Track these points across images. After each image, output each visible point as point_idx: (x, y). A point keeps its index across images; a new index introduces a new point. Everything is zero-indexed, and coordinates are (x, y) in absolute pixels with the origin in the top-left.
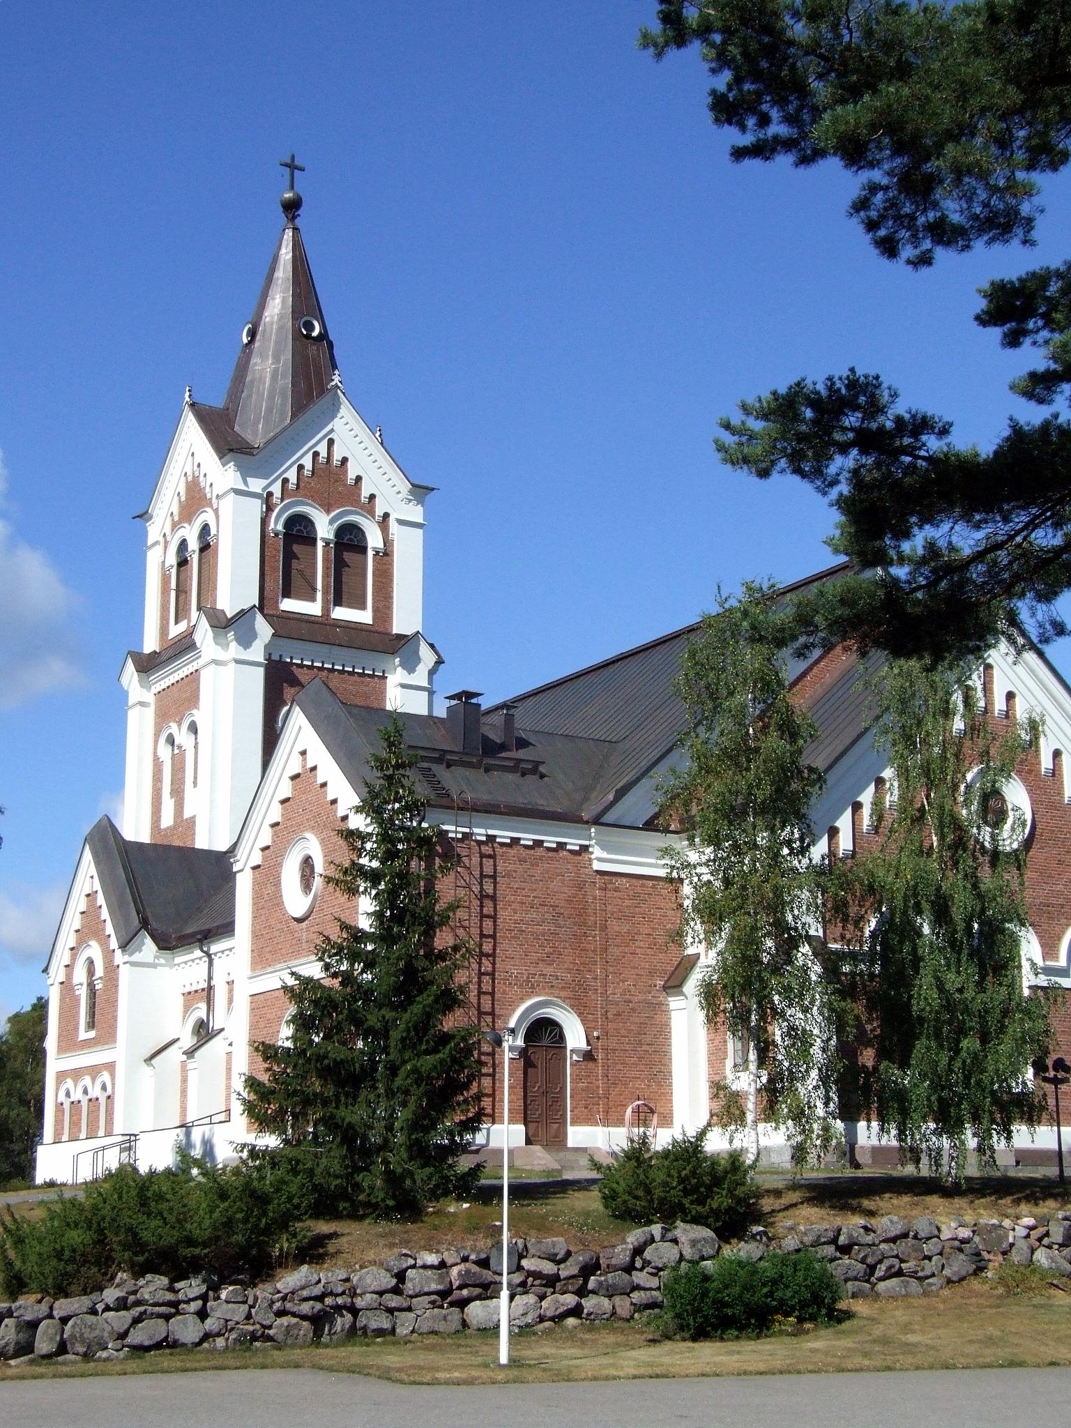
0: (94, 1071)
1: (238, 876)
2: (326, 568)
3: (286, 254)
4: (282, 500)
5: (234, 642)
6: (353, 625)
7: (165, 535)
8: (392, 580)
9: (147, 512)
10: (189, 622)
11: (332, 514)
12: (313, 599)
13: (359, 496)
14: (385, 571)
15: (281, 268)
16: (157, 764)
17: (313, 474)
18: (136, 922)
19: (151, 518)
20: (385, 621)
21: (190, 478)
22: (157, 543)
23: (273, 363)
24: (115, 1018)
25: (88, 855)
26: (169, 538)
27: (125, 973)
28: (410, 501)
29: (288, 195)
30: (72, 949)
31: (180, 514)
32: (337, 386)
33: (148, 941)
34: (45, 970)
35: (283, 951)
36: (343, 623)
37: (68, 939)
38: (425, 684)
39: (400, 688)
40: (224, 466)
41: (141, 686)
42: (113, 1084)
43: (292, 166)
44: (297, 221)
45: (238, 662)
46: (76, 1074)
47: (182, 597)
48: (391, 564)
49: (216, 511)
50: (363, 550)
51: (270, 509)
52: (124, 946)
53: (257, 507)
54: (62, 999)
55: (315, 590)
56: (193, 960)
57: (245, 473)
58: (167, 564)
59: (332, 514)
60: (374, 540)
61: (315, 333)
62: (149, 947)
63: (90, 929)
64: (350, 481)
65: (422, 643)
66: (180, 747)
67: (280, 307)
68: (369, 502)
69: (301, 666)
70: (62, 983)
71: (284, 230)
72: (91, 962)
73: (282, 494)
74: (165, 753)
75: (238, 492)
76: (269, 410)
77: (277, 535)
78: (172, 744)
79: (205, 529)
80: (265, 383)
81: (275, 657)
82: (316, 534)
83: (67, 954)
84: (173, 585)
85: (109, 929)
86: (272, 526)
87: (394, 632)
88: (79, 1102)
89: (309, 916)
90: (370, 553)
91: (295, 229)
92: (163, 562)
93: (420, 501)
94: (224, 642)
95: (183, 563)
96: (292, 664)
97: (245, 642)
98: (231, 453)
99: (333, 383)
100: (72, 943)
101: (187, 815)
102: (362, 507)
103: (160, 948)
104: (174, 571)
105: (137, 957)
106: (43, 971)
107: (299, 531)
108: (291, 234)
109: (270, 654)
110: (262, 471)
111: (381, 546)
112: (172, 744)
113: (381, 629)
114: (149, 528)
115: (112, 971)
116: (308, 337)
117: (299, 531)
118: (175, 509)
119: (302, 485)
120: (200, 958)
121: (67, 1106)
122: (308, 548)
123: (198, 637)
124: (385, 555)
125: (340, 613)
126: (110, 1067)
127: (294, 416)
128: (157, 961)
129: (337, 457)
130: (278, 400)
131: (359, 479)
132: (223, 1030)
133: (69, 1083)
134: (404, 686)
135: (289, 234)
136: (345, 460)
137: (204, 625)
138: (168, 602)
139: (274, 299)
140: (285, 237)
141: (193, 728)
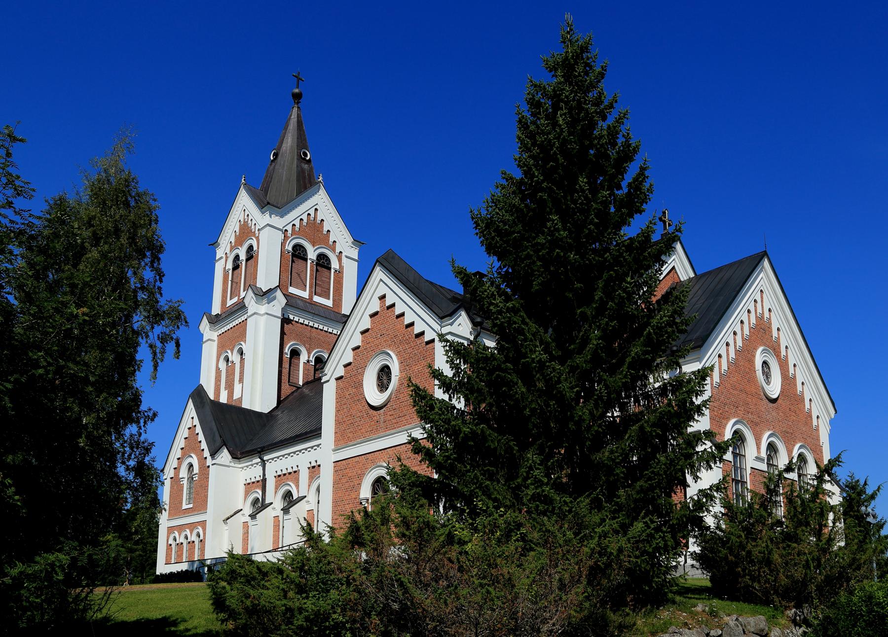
0: (192, 526)
2: (311, 275)
6: (323, 306)
10: (239, 296)
12: (305, 290)
13: (329, 241)
15: (292, 125)
16: (218, 371)
19: (219, 245)
21: (242, 223)
22: (221, 258)
24: (206, 497)
25: (191, 405)
26: (228, 255)
29: (297, 91)
30: (179, 459)
31: (236, 242)
35: (363, 430)
37: (176, 453)
42: (204, 534)
46: (180, 528)
47: (234, 285)
52: (213, 454)
56: (252, 465)
60: (335, 265)
61: (308, 158)
62: (225, 456)
63: (191, 445)
70: (172, 478)
72: (191, 466)
74: (223, 365)
78: (228, 361)
79: (251, 248)
81: (286, 316)
83: (176, 461)
84: (230, 278)
85: (204, 445)
88: (182, 543)
89: (385, 406)
90: (333, 271)
95: (236, 267)
103: (233, 458)
104: (230, 272)
107: (299, 253)
109: (283, 314)
111: (338, 267)
112: (228, 361)
114: (217, 251)
115: (205, 469)
116: (304, 159)
117: (299, 253)
118: (233, 240)
120: (257, 464)
123: (246, 302)
124: (339, 273)
125: (316, 299)
126: (203, 524)
129: (319, 219)
132: (272, 503)
135: (295, 110)
141: (241, 352)
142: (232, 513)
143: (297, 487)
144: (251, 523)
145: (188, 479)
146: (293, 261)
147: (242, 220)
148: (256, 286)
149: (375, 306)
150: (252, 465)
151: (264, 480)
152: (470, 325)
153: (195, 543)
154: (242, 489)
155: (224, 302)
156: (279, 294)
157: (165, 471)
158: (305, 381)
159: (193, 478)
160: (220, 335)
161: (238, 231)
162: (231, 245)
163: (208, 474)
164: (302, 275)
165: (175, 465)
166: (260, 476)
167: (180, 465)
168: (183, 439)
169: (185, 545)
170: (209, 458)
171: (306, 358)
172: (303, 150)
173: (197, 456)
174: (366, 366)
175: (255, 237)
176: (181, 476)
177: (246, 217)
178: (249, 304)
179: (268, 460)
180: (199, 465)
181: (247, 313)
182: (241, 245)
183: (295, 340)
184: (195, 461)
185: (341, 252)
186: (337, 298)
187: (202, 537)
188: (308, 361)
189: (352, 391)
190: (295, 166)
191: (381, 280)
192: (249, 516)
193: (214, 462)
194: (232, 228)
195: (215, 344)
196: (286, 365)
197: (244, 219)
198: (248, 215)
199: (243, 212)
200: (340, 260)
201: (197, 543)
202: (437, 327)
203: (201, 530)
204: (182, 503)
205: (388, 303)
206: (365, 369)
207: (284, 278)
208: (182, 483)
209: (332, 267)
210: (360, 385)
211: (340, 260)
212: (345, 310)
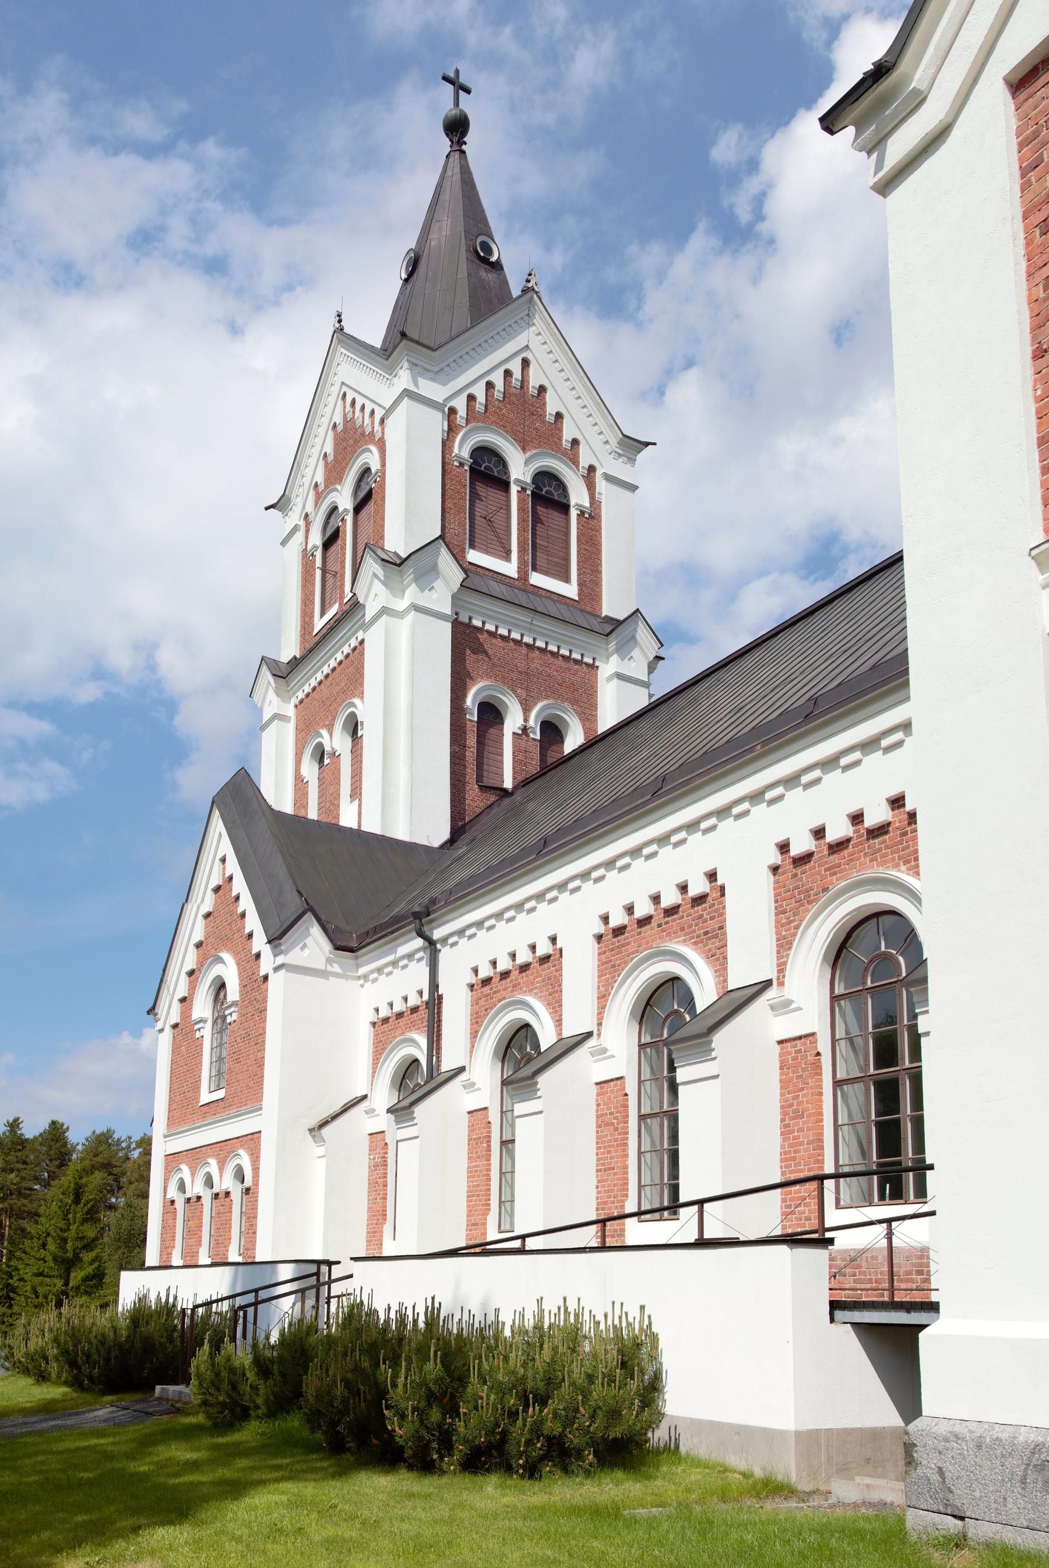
0: (223, 1149)
4: (468, 421)
13: (560, 438)
17: (504, 397)
18: (295, 905)
24: (260, 1064)
25: (218, 826)
26: (311, 518)
27: (277, 987)
28: (620, 455)
33: (316, 931)
34: (152, 1011)
37: (185, 957)
42: (256, 1170)
46: (195, 1156)
47: (330, 582)
51: (452, 429)
52: (275, 939)
53: (437, 423)
54: (176, 1050)
59: (529, 454)
60: (578, 496)
64: (550, 418)
69: (493, 634)
74: (310, 771)
77: (462, 465)
81: (464, 618)
82: (509, 477)
83: (184, 979)
84: (319, 563)
85: (253, 923)
86: (456, 450)
90: (574, 513)
95: (331, 540)
96: (480, 630)
100: (190, 964)
101: (356, 802)
102: (564, 453)
104: (319, 554)
105: (295, 956)
106: (148, 1012)
110: (439, 375)
111: (587, 503)
119: (491, 409)
120: (410, 956)
121: (180, 1205)
125: (537, 579)
126: (252, 1141)
128: (329, 968)
129: (534, 380)
133: (185, 1172)
134: (620, 676)
138: (313, 593)
141: (354, 728)
142: (337, 1107)
143: (555, 1006)
144: (394, 1133)
145: (215, 1022)
146: (474, 496)
150: (394, 964)
151: (434, 1004)
153: (233, 1196)
154: (364, 1037)
156: (445, 559)
157: (157, 1010)
158: (520, 778)
159: (224, 1017)
160: (301, 702)
163: (265, 1000)
164: (498, 520)
165: (182, 991)
166: (421, 993)
167: (192, 988)
168: (200, 918)
169: (207, 1201)
170: (266, 951)
171: (520, 722)
172: (481, 239)
173: (235, 954)
176: (195, 1016)
177: (348, 408)
178: (366, 597)
179: (444, 940)
180: (241, 979)
183: (489, 676)
184: (229, 970)
185: (592, 469)
186: (587, 578)
187: (248, 1182)
188: (525, 730)
190: (463, 274)
192: (389, 1111)
193: (280, 960)
195: (290, 728)
196: (472, 741)
199: (340, 402)
200: (591, 486)
201: (236, 1196)
203: (245, 1160)
204: (199, 1088)
207: (453, 526)
208: (198, 1035)
209: (573, 502)
211: (591, 486)
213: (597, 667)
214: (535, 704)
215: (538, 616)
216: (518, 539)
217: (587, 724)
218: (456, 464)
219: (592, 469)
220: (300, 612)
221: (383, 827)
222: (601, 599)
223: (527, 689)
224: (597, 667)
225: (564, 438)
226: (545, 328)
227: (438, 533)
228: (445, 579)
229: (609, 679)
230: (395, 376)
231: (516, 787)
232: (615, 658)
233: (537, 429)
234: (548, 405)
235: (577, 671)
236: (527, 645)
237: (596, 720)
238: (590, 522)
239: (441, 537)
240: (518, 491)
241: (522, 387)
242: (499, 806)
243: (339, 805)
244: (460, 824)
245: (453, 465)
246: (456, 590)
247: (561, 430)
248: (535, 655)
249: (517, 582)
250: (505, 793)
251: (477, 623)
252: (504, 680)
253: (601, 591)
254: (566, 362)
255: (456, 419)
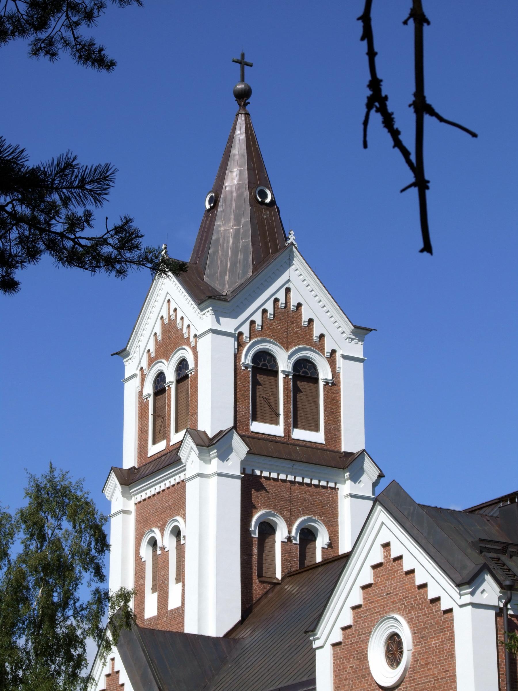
1: (317, 652)
2: (286, 396)
3: (240, 134)
4: (250, 338)
5: (217, 459)
6: (309, 445)
7: (142, 368)
8: (339, 407)
9: (125, 349)
11: (291, 351)
12: (276, 423)
13: (312, 336)
14: (334, 399)
15: (237, 146)
19: (128, 354)
20: (335, 441)
21: (166, 321)
22: (134, 376)
23: (235, 225)
26: (145, 372)
28: (353, 339)
29: (240, 86)
31: (157, 351)
32: (292, 244)
36: (301, 443)
38: (370, 495)
39: (349, 498)
40: (202, 310)
41: (123, 496)
43: (242, 63)
44: (248, 107)
45: (219, 475)
47: (159, 421)
48: (338, 393)
49: (194, 350)
50: (315, 380)
51: (240, 345)
53: (230, 344)
55: (278, 415)
57: (218, 314)
58: (145, 393)
59: (291, 351)
61: (268, 200)
64: (304, 324)
65: (367, 459)
66: (163, 548)
67: (237, 178)
68: (320, 340)
69: (268, 478)
71: (237, 115)
73: (250, 334)
74: (146, 553)
75: (215, 332)
76: (234, 264)
77: (247, 368)
79: (183, 364)
80: (228, 242)
81: (248, 471)
82: (277, 368)
86: (243, 360)
87: (343, 450)
89: (402, 682)
90: (321, 384)
91: (247, 114)
92: (141, 393)
93: (361, 339)
94: (208, 458)
96: (260, 477)
97: (223, 456)
98: (210, 300)
99: (289, 241)
101: (180, 584)
102: (314, 345)
104: (151, 400)
108: (243, 118)
111: (330, 377)
113: (332, 448)
114: (126, 364)
116: (263, 203)
118: (152, 346)
119: (266, 326)
122: (270, 379)
123: (183, 454)
125: (299, 434)
127: (255, 269)
129: (293, 303)
130: (240, 256)
131: (311, 321)
135: (242, 118)
136: (299, 305)
137: (189, 443)
138: (147, 425)
139: (232, 172)
140: (239, 121)
141: (177, 533)
147: (166, 317)
148: (196, 430)
149: (377, 557)
152: (497, 589)
155: (142, 448)
158: (286, 571)
160: (140, 502)
161: (159, 333)
162: (149, 356)
171: (286, 534)
174: (370, 632)
175: (190, 347)
177: (172, 312)
181: (185, 470)
182: (167, 358)
183: (265, 506)
185: (333, 352)
186: (331, 428)
188: (289, 539)
189: (354, 663)
191: (383, 523)
194: (149, 328)
195: (132, 519)
197: (170, 316)
198: (175, 310)
202: (456, 596)
205: (394, 554)
206: (369, 636)
210: (363, 657)
212: (344, 548)
213: (338, 489)
214: (296, 520)
215: (297, 463)
216: (284, 409)
217: (331, 529)
218: (243, 368)
219: (333, 352)
220: (137, 435)
221: (199, 628)
222: (340, 440)
223: (290, 511)
224: (338, 489)
225: (314, 335)
226: (300, 266)
227: (232, 425)
228: (237, 453)
229: (346, 496)
230: (204, 314)
231: (283, 578)
232: (349, 482)
233: (296, 333)
234: (303, 315)
235: (324, 494)
236: (290, 482)
237: (337, 525)
238: (332, 388)
239: (235, 427)
240: (284, 378)
241: (286, 307)
242: (273, 591)
243: (168, 585)
244: (247, 606)
245: (241, 369)
246: (243, 458)
247: (312, 330)
248: (295, 487)
249: (283, 439)
250: (276, 584)
251: (258, 473)
252: (275, 508)
253: (340, 433)
254: (315, 285)
255: (243, 338)
